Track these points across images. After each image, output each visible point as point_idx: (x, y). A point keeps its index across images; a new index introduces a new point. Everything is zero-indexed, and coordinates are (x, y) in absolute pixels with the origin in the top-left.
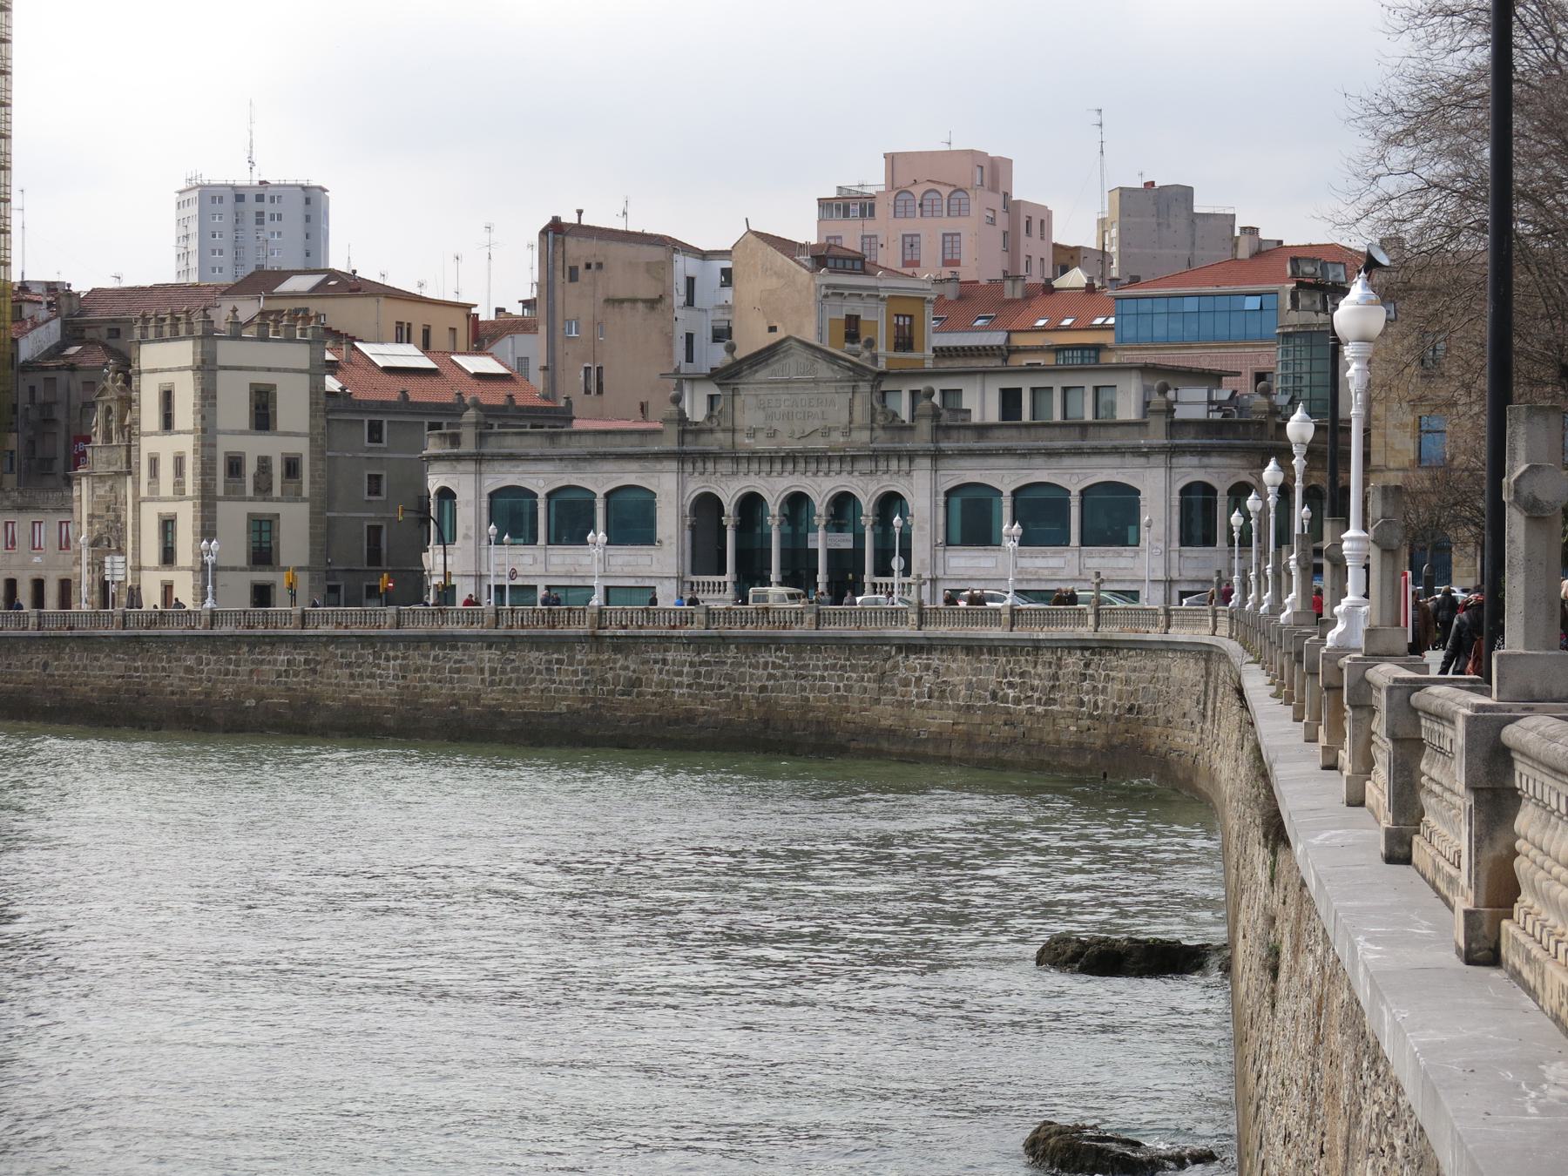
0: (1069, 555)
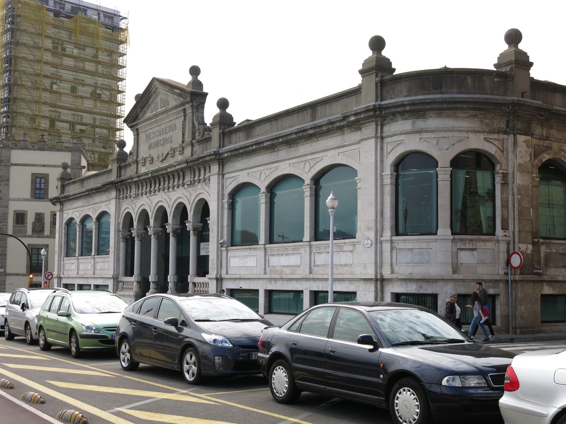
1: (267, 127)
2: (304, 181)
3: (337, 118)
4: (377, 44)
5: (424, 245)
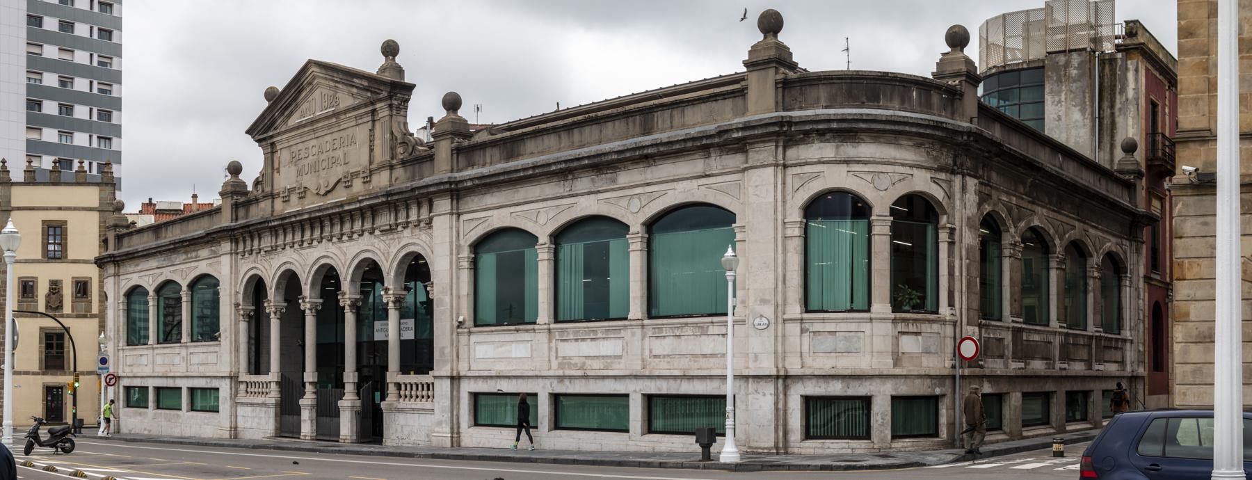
0: (626, 334)
4: (771, 23)
5: (853, 327)
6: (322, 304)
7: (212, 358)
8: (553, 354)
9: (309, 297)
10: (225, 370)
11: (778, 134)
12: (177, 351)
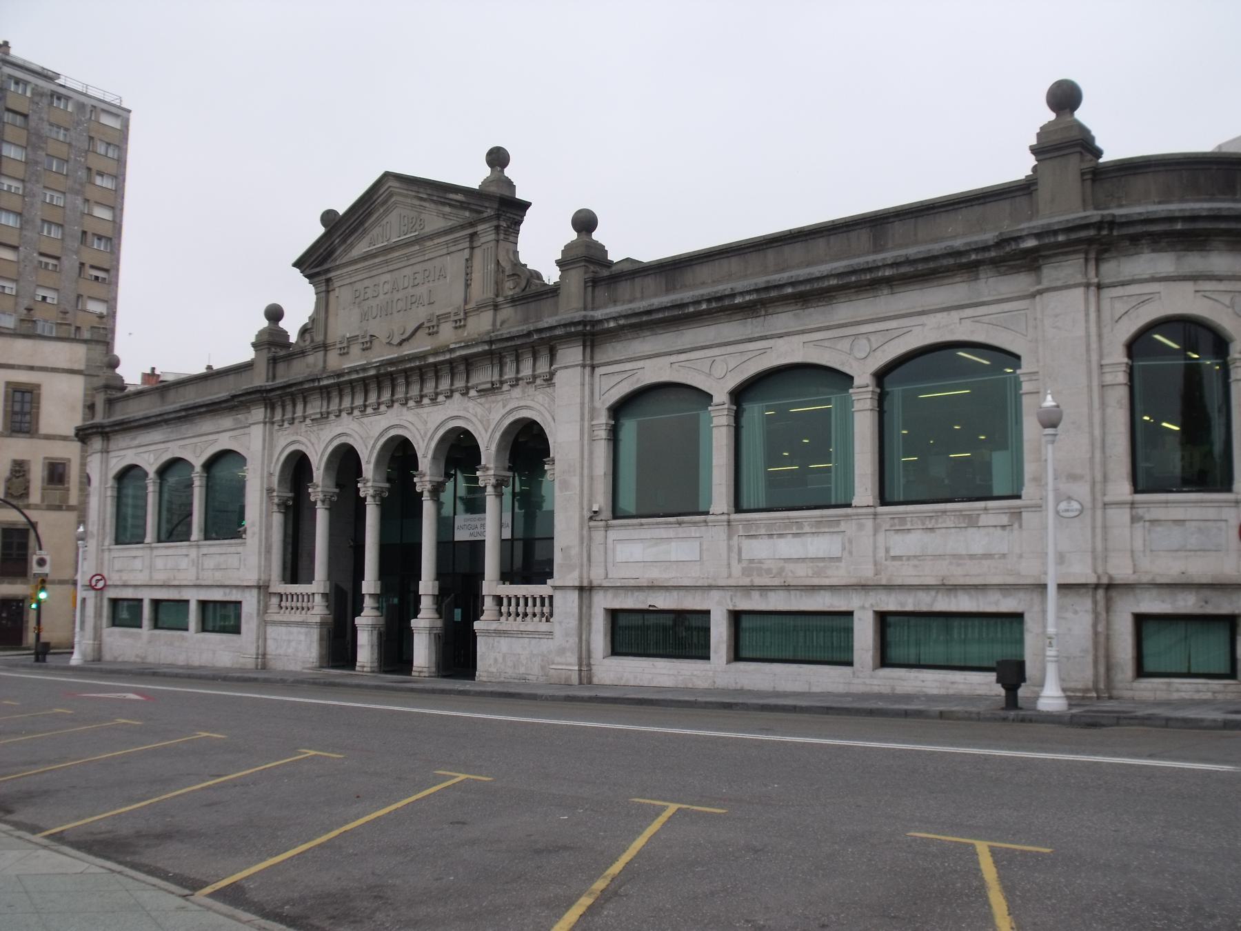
0: (849, 527)
1: (734, 264)
2: (852, 378)
3: (1060, 222)
4: (1065, 97)
5: (1211, 513)
6: (389, 490)
7: (233, 561)
8: (735, 556)
9: (370, 482)
10: (252, 577)
11: (1089, 241)
12: (184, 551)
